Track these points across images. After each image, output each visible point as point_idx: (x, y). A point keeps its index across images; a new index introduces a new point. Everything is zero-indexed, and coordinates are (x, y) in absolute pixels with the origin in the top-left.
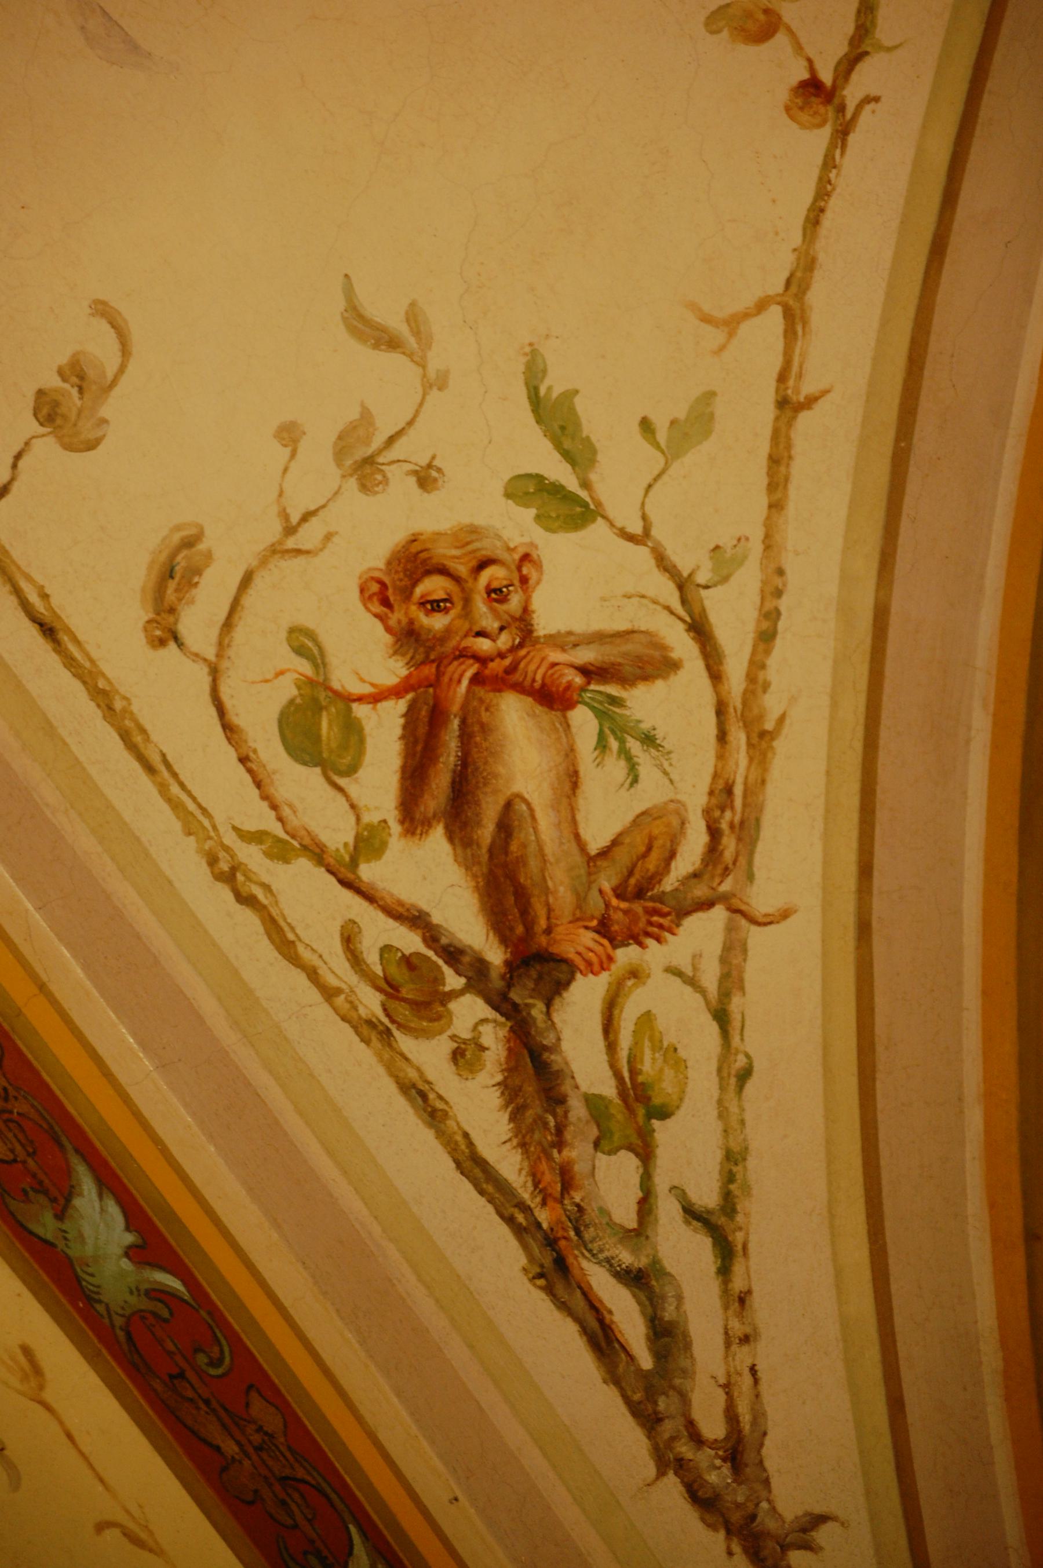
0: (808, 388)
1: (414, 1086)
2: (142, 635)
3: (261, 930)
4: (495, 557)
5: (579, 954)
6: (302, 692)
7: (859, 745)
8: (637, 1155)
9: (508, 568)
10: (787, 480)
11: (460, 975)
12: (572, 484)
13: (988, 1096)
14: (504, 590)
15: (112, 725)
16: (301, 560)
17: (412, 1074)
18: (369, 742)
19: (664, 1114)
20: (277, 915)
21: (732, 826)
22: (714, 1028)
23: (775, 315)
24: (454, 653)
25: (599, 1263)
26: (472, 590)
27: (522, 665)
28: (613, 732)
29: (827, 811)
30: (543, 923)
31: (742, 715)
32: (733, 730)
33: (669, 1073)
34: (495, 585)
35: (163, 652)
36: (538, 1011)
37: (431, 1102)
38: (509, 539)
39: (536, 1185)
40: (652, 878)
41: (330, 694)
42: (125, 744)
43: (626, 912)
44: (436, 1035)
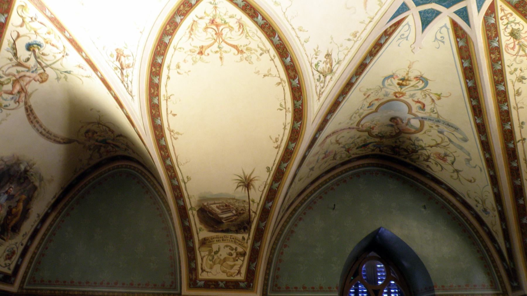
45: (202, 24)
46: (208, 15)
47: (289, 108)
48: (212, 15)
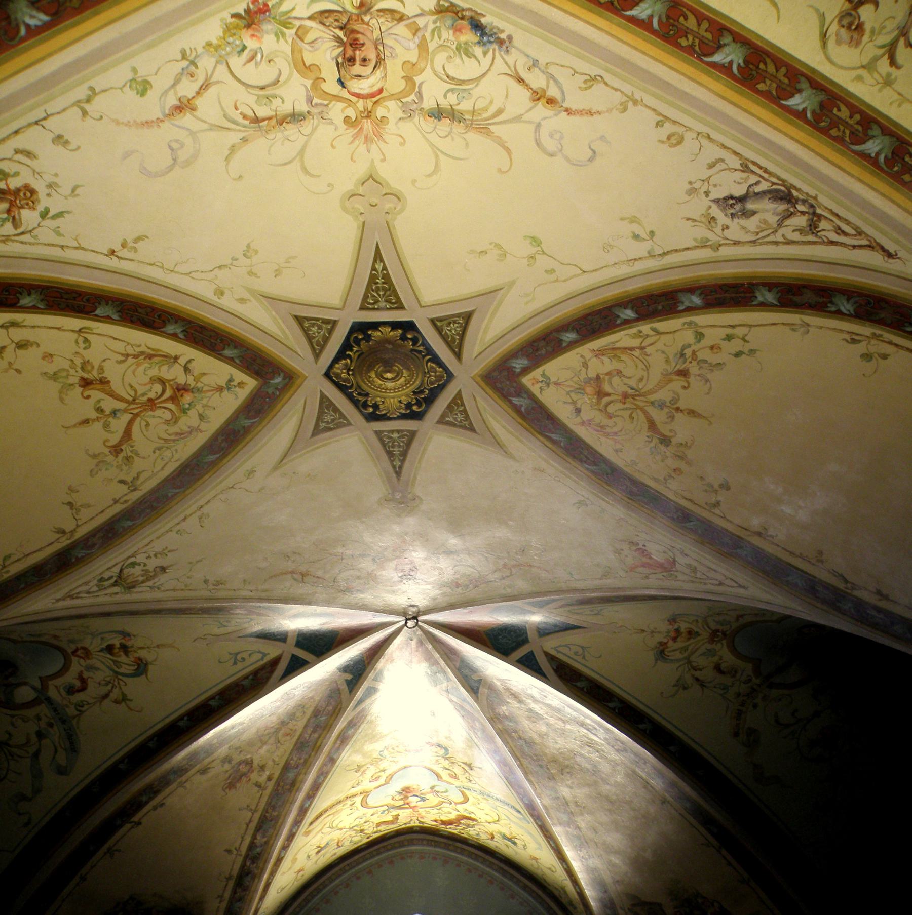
23: (78, 245)
45: (176, 374)
46: (197, 380)
47: (8, 572)
48: (199, 385)
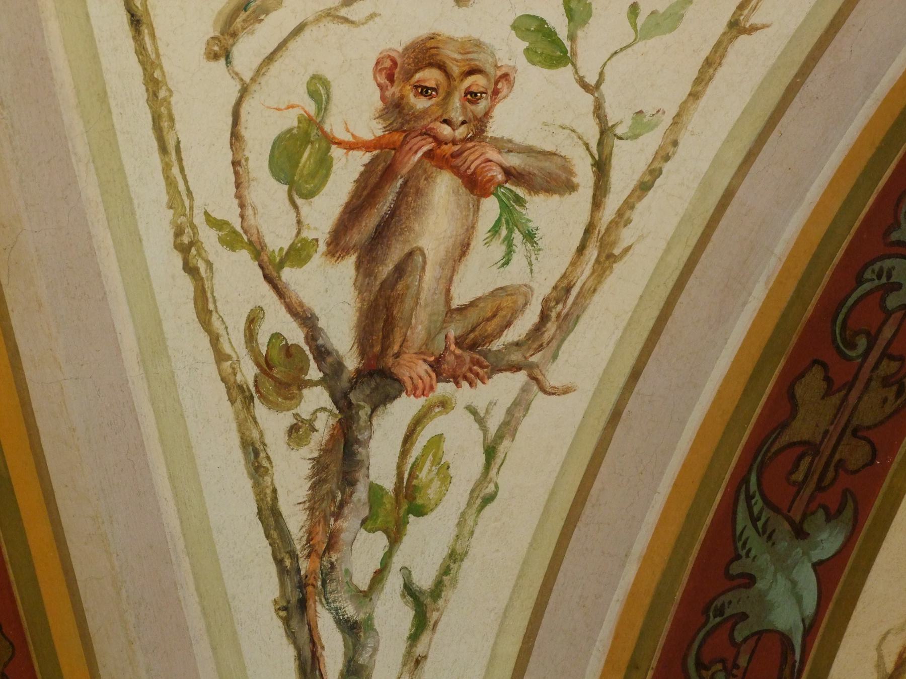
0: (755, 19)
1: (253, 444)
2: (204, 46)
3: (192, 295)
4: (483, 68)
5: (411, 378)
6: (301, 125)
7: (671, 284)
8: (388, 537)
9: (489, 80)
10: (710, 79)
11: (320, 371)
12: (562, 33)
13: (647, 559)
14: (479, 95)
15: (151, 108)
16: (345, 27)
17: (255, 435)
18: (332, 177)
19: (420, 512)
20: (208, 287)
21: (558, 316)
22: (482, 459)
24: (422, 130)
25: (329, 610)
26: (456, 88)
27: (465, 154)
28: (507, 223)
29: (629, 324)
30: (396, 348)
31: (602, 238)
32: (591, 246)
33: (436, 484)
34: (474, 89)
35: (213, 64)
36: (363, 414)
37: (259, 459)
38: (499, 59)
39: (308, 541)
40: (486, 337)
41: (320, 133)
42: (154, 125)
43: (457, 357)
44: (284, 411)
